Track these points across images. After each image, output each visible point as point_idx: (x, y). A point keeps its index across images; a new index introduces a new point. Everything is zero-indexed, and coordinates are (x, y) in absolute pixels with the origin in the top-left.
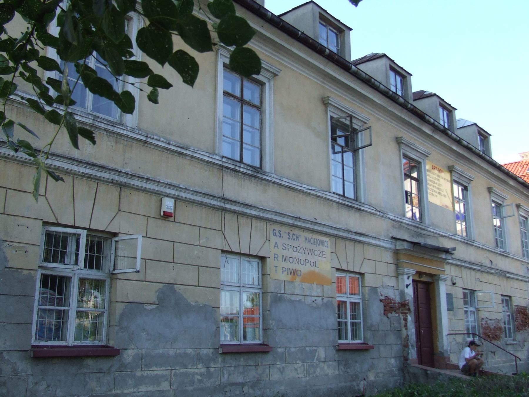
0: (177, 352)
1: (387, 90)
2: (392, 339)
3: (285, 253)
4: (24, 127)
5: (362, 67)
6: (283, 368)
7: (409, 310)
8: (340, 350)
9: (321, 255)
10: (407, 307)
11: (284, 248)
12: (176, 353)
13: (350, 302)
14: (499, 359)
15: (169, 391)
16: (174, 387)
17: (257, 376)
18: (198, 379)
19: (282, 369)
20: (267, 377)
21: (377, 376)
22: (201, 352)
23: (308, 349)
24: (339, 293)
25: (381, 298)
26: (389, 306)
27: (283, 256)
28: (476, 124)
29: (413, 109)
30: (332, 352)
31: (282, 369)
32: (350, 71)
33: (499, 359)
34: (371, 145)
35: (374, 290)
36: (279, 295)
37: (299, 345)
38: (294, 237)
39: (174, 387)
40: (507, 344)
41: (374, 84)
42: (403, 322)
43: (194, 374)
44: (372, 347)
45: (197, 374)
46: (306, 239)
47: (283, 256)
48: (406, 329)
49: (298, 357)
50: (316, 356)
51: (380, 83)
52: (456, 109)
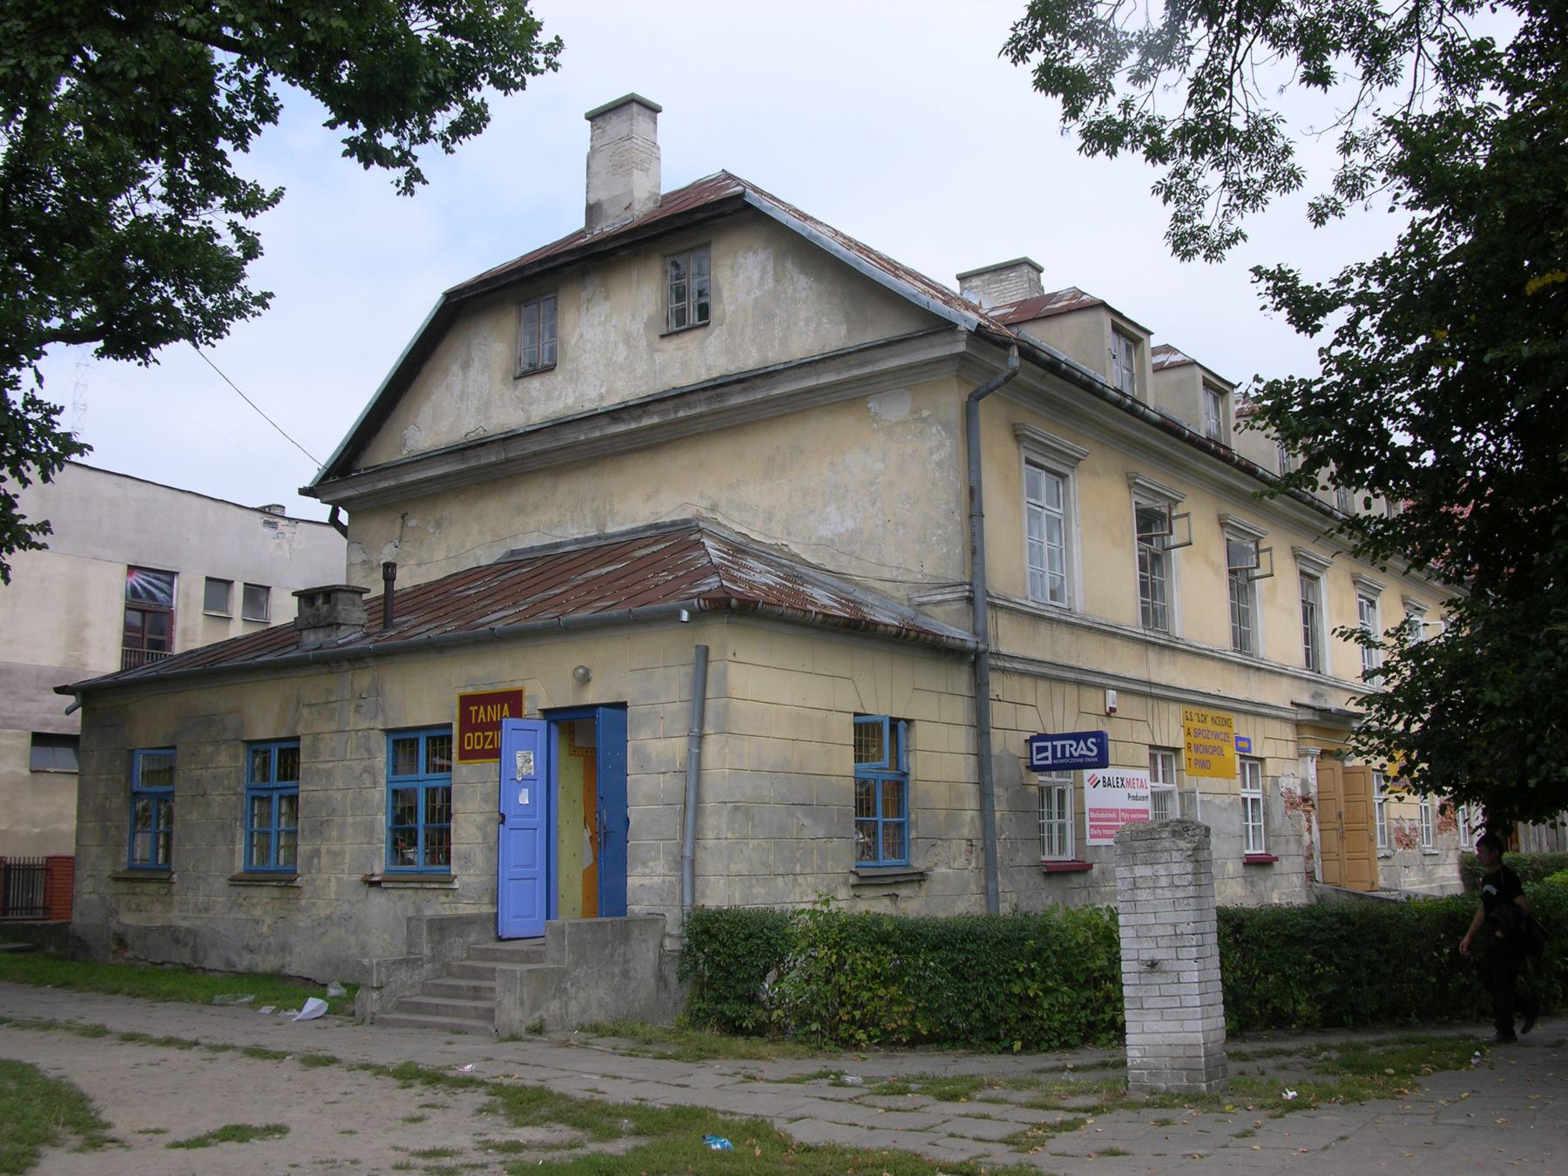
44: (1276, 859)
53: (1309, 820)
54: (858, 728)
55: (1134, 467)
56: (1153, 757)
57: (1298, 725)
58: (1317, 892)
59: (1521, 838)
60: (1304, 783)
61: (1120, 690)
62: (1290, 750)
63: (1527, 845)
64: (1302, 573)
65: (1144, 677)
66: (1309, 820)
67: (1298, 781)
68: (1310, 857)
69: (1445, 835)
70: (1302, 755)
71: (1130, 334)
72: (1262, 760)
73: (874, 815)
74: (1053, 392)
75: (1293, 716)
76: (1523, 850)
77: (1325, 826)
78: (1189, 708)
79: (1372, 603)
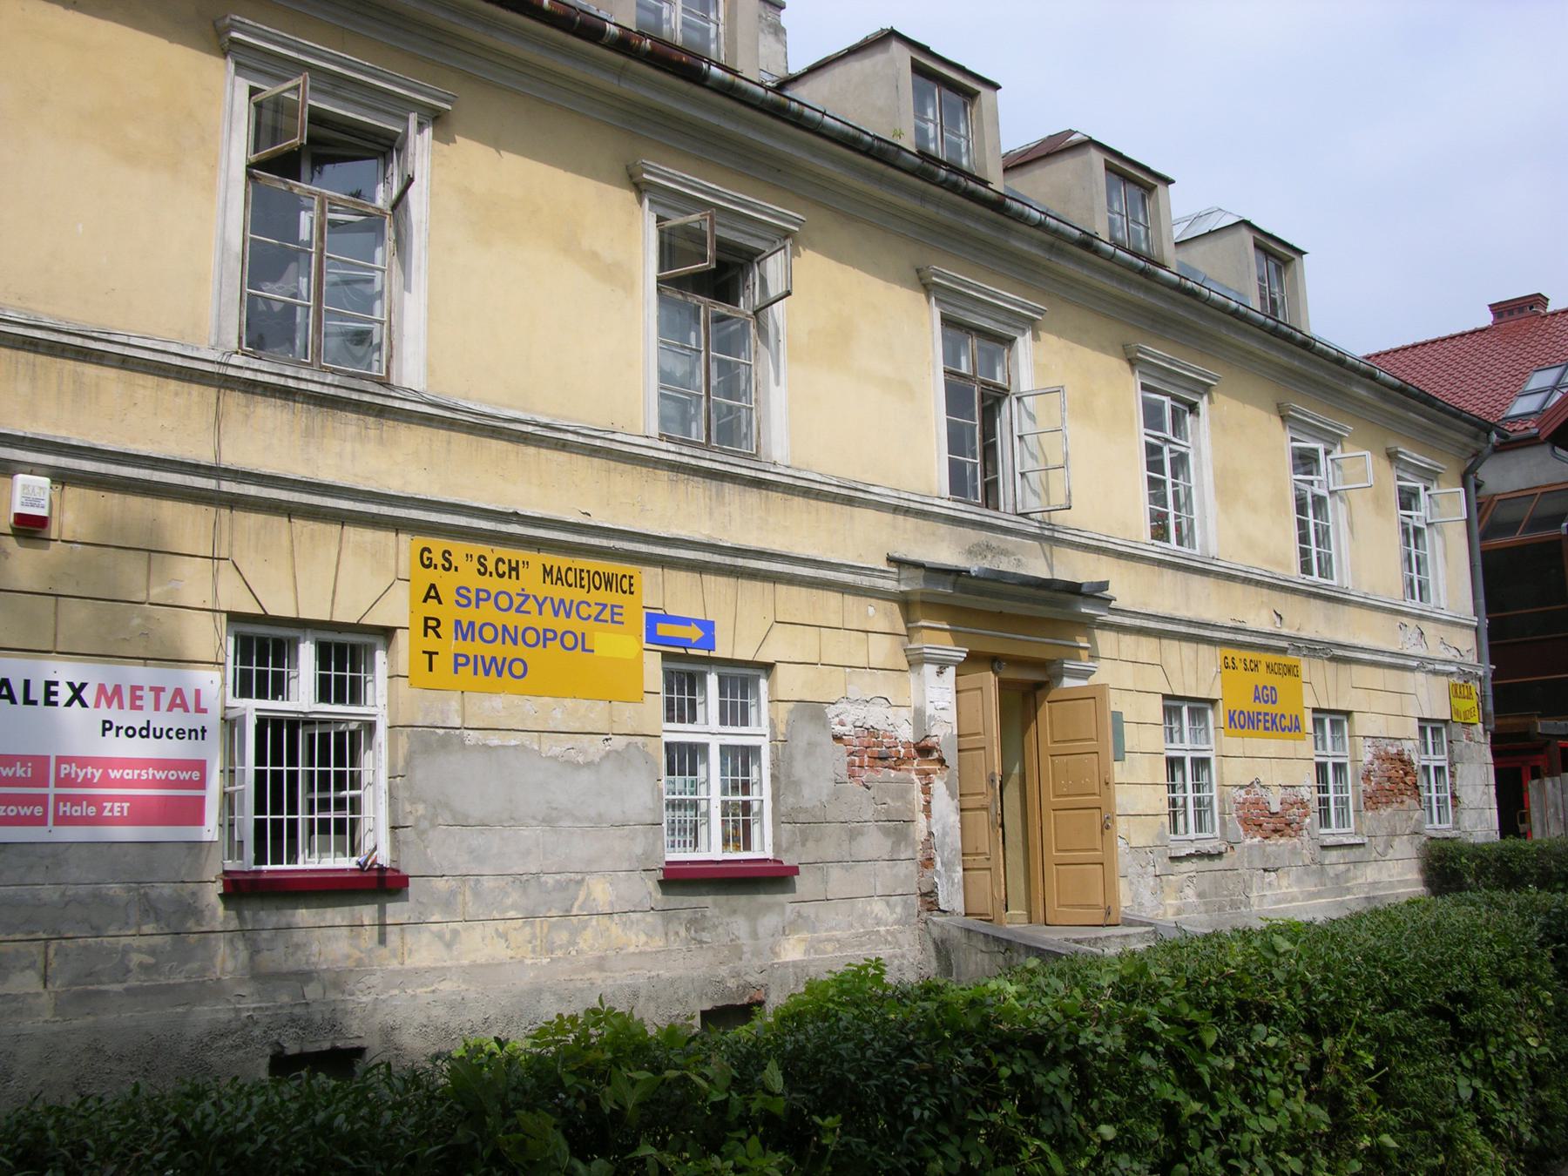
0: (69, 893)
1: (728, 77)
2: (873, 843)
3: (466, 615)
4: (1210, 856)
5: (800, 92)
6: (455, 933)
7: (942, 761)
8: (678, 880)
9: (606, 615)
10: (936, 755)
11: (464, 602)
12: (63, 894)
13: (724, 749)
14: (1295, 889)
15: (38, 995)
16: (57, 985)
17: (357, 954)
18: (141, 965)
19: (448, 937)
20: (395, 956)
21: (812, 947)
22: (153, 894)
23: (550, 880)
24: (670, 719)
25: (839, 729)
26: (875, 753)
27: (458, 623)
28: (1246, 224)
29: (1276, 328)
30: (647, 889)
31: (448, 937)
32: (605, 40)
33: (1295, 889)
34: (788, 293)
35: (813, 711)
36: (441, 731)
37: (516, 870)
38: (503, 568)
39: (57, 985)
40: (1323, 847)
41: (800, 115)
42: (918, 798)
43: (126, 950)
44: (795, 870)
45: (139, 950)
46: (547, 572)
47: (458, 623)
48: (928, 816)
49: (509, 901)
50: (581, 898)
51: (824, 114)
52: (1168, 181)
53: (926, 790)
54: (245, 647)
55: (1393, 443)
56: (1422, 730)
57: (906, 604)
58: (936, 932)
59: (1535, 814)
60: (919, 717)
61: (61, 478)
62: (882, 650)
63: (1544, 825)
64: (947, 321)
65: (206, 457)
66: (926, 790)
67: (906, 714)
68: (928, 862)
69: (1385, 812)
70: (916, 661)
71: (1137, 180)
72: (1348, 714)
73: (46, 796)
74: (713, 120)
75: (890, 585)
76: (1537, 834)
77: (970, 802)
78: (1231, 652)
79: (1193, 408)
